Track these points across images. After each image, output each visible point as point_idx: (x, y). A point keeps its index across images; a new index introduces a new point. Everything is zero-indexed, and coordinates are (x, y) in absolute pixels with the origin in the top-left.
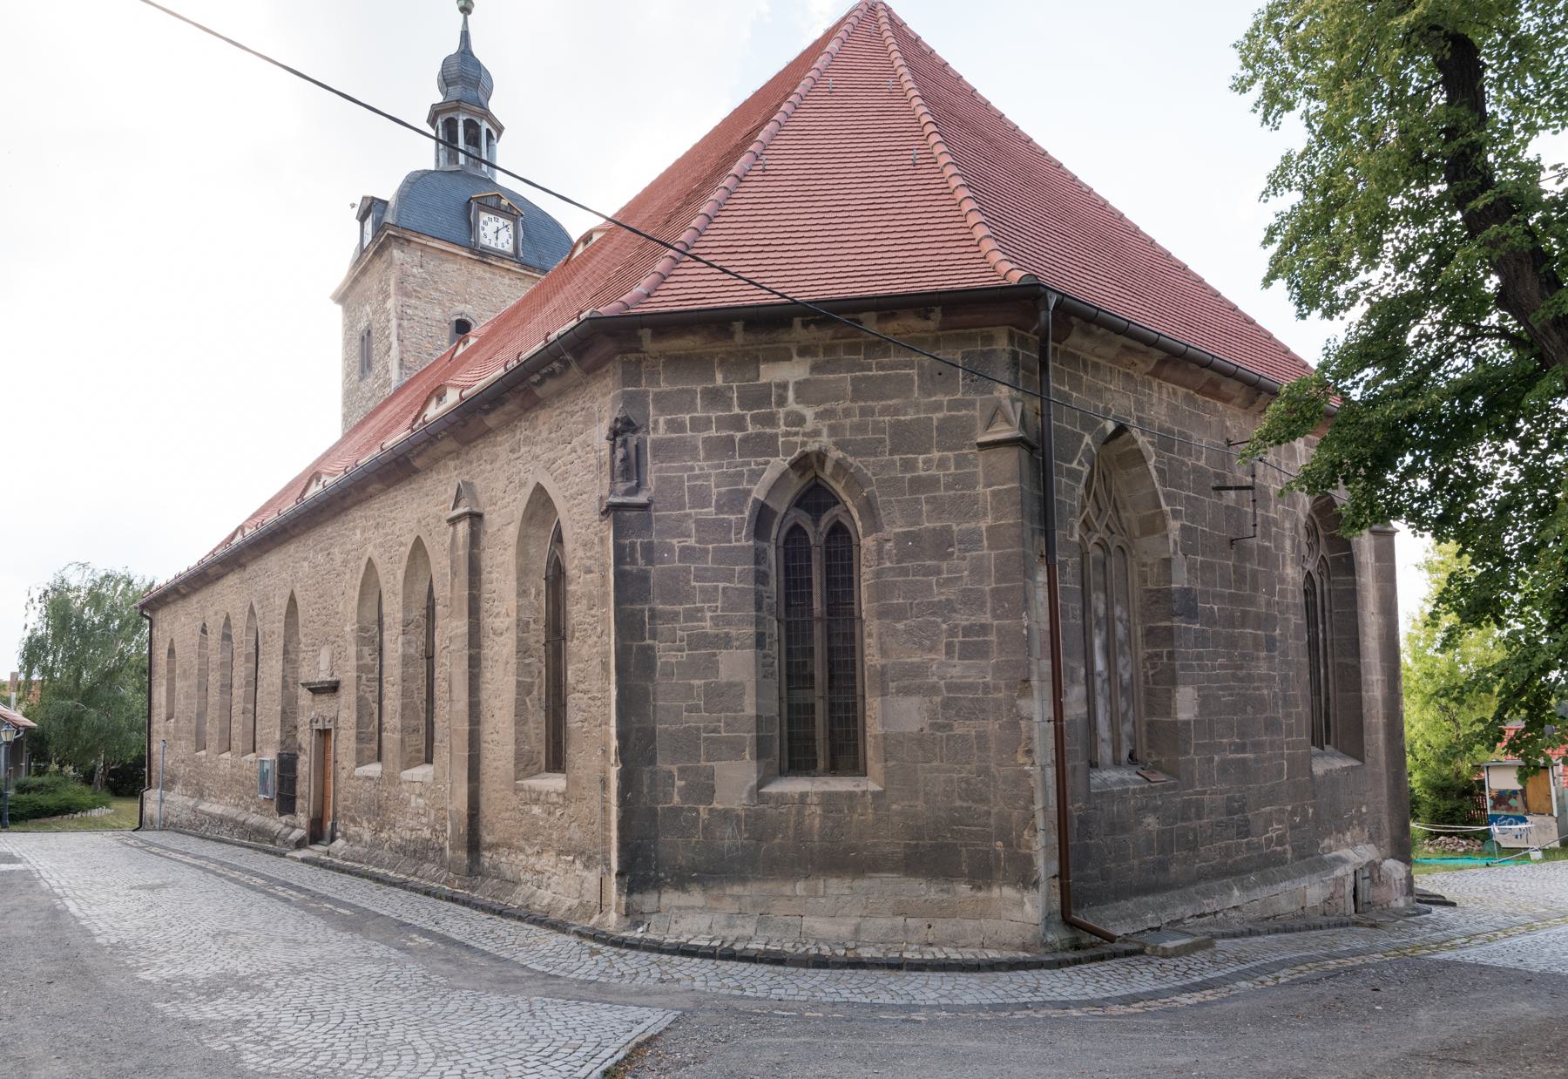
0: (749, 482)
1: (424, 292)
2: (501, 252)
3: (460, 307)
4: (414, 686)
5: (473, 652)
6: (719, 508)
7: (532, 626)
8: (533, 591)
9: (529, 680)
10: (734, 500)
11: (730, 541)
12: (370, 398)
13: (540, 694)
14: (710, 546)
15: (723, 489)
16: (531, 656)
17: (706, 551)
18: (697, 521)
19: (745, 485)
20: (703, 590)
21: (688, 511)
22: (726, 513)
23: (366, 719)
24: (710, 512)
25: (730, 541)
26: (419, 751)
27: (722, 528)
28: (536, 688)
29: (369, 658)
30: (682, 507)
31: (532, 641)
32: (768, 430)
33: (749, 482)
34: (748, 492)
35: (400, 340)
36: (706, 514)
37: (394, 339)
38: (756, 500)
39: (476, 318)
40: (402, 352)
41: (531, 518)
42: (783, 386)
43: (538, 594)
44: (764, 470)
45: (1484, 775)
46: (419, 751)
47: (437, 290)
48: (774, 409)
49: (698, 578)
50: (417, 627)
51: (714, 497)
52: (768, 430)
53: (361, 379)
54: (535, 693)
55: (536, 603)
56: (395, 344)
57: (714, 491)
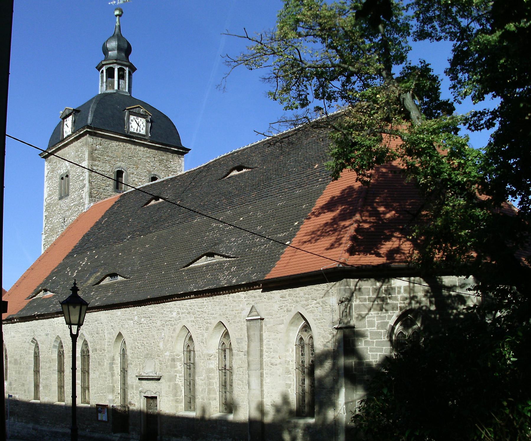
0: (388, 319)
1: (102, 157)
2: (139, 134)
3: (119, 164)
4: (214, 381)
5: (62, 350)
6: (378, 328)
7: (291, 363)
8: (291, 350)
9: (290, 383)
10: (383, 325)
11: (382, 339)
12: (68, 210)
13: (294, 388)
14: (375, 341)
15: (379, 321)
16: (291, 374)
17: (373, 342)
18: (370, 332)
19: (386, 320)
20: (372, 355)
21: (367, 328)
22: (380, 329)
23: (179, 393)
24: (375, 329)
25: (382, 339)
26: (216, 408)
27: (378, 334)
28: (292, 386)
29: (179, 367)
30: (365, 327)
31: (290, 369)
32: (394, 302)
33: (388, 319)
34: (388, 323)
35: (90, 182)
36: (373, 330)
37: (86, 182)
38: (390, 325)
39: (125, 168)
40: (91, 189)
41: (292, 323)
42: (400, 288)
43: (293, 351)
44: (393, 315)
45: (211, 401)
46: (216, 408)
47: (108, 156)
48: (397, 295)
49: (371, 351)
50: (215, 357)
51: (376, 324)
52: (394, 302)
53: (61, 198)
54: (292, 387)
55: (292, 354)
56: (87, 185)
57: (376, 322)
